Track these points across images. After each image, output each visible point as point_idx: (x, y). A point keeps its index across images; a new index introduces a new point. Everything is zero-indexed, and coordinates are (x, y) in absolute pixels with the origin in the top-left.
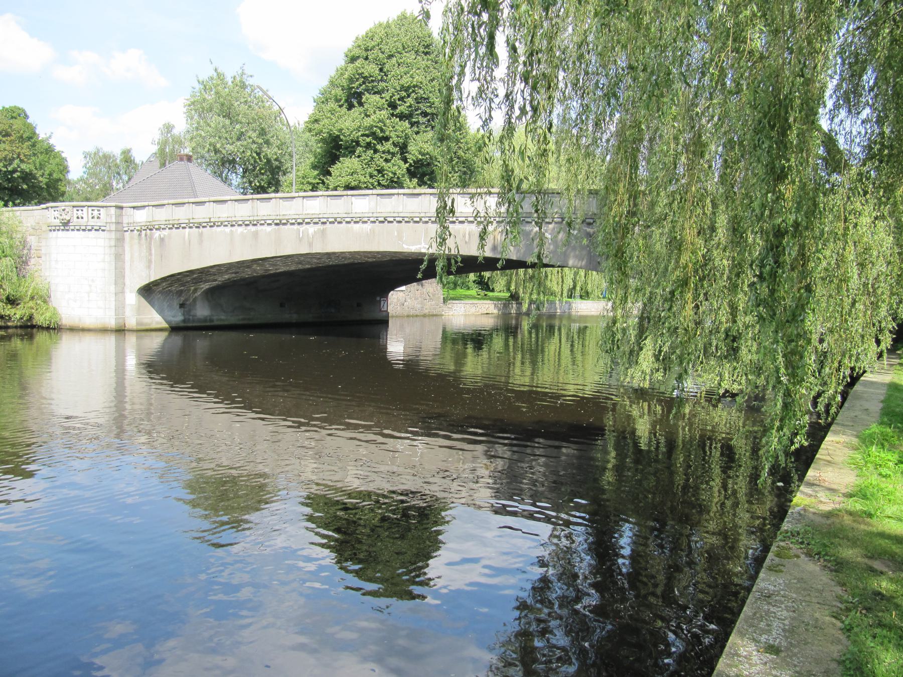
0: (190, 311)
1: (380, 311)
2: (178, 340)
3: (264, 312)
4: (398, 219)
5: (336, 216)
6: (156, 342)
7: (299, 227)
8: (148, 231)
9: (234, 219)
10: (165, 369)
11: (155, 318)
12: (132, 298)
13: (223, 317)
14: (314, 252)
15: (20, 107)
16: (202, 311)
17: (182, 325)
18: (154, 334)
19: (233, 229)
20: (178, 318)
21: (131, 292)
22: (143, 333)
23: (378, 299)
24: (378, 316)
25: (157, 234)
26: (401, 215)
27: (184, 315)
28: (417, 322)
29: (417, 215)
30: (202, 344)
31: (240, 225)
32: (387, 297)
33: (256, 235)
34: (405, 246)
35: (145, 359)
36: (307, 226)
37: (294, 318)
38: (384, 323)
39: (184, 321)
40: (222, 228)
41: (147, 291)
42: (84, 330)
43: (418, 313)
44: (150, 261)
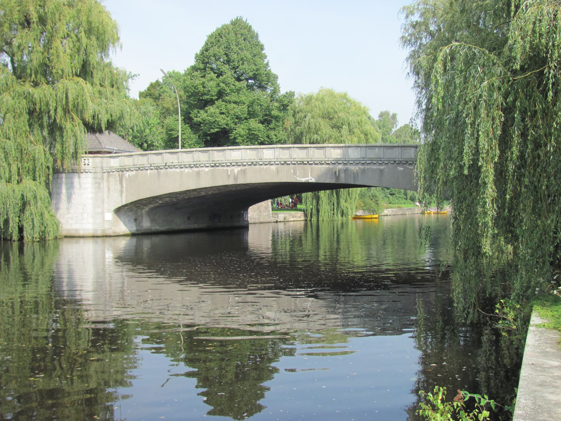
0: (139, 224)
1: (244, 220)
2: (134, 240)
3: (179, 223)
4: (293, 162)
5: (253, 161)
6: (123, 243)
7: (227, 168)
8: (120, 172)
9: (183, 164)
10: (132, 260)
11: (123, 228)
12: (110, 216)
14: (239, 183)
15: (262, 39)
16: (146, 224)
17: (136, 232)
18: (121, 238)
19: (182, 170)
20: (134, 229)
21: (108, 212)
22: (105, 238)
23: (242, 212)
24: (242, 224)
25: (127, 174)
26: (296, 160)
27: (137, 227)
28: (265, 225)
29: (306, 160)
30: (147, 243)
31: (187, 167)
32: (247, 210)
33: (198, 173)
34: (298, 178)
35: (117, 255)
36: (233, 168)
37: (196, 226)
38: (246, 228)
39: (137, 230)
40: (174, 170)
41: (118, 211)
42: (110, 236)
43: (257, 221)
44: (122, 192)
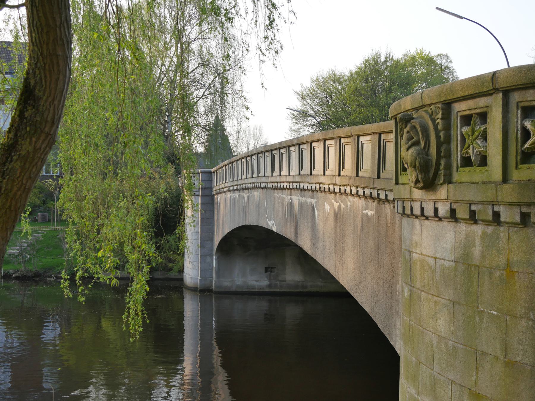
13: (319, 284)
39: (270, 286)
